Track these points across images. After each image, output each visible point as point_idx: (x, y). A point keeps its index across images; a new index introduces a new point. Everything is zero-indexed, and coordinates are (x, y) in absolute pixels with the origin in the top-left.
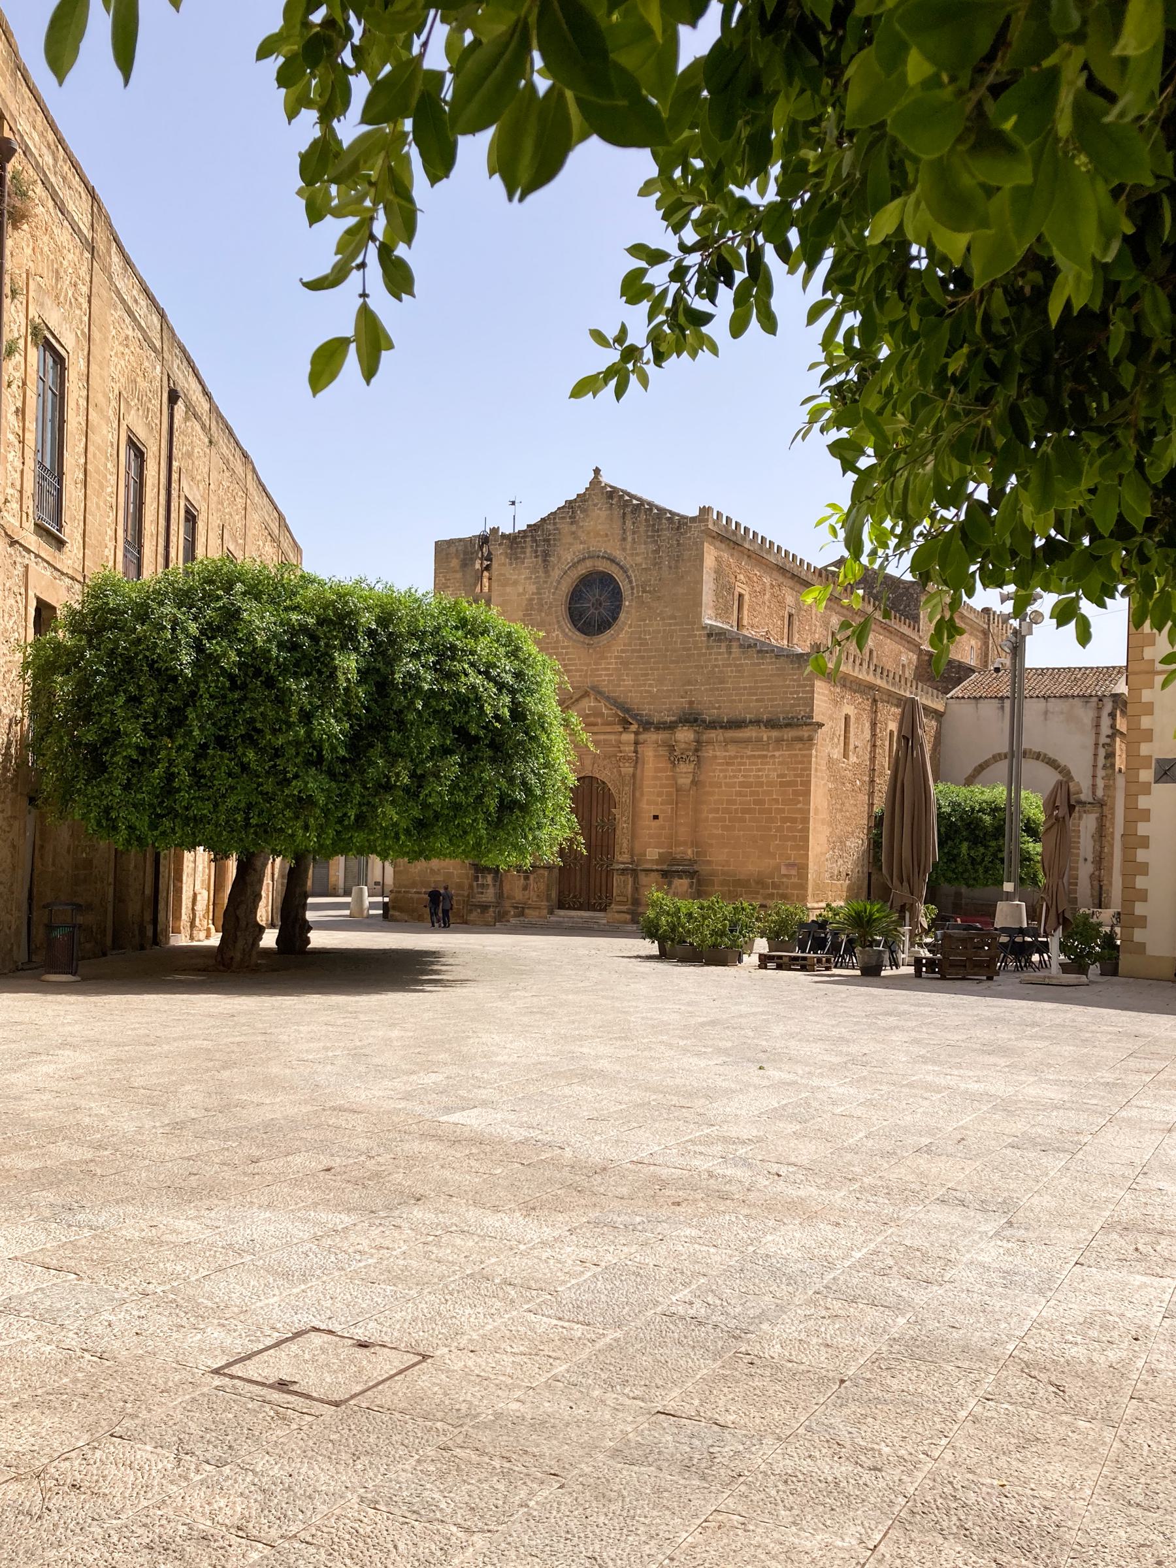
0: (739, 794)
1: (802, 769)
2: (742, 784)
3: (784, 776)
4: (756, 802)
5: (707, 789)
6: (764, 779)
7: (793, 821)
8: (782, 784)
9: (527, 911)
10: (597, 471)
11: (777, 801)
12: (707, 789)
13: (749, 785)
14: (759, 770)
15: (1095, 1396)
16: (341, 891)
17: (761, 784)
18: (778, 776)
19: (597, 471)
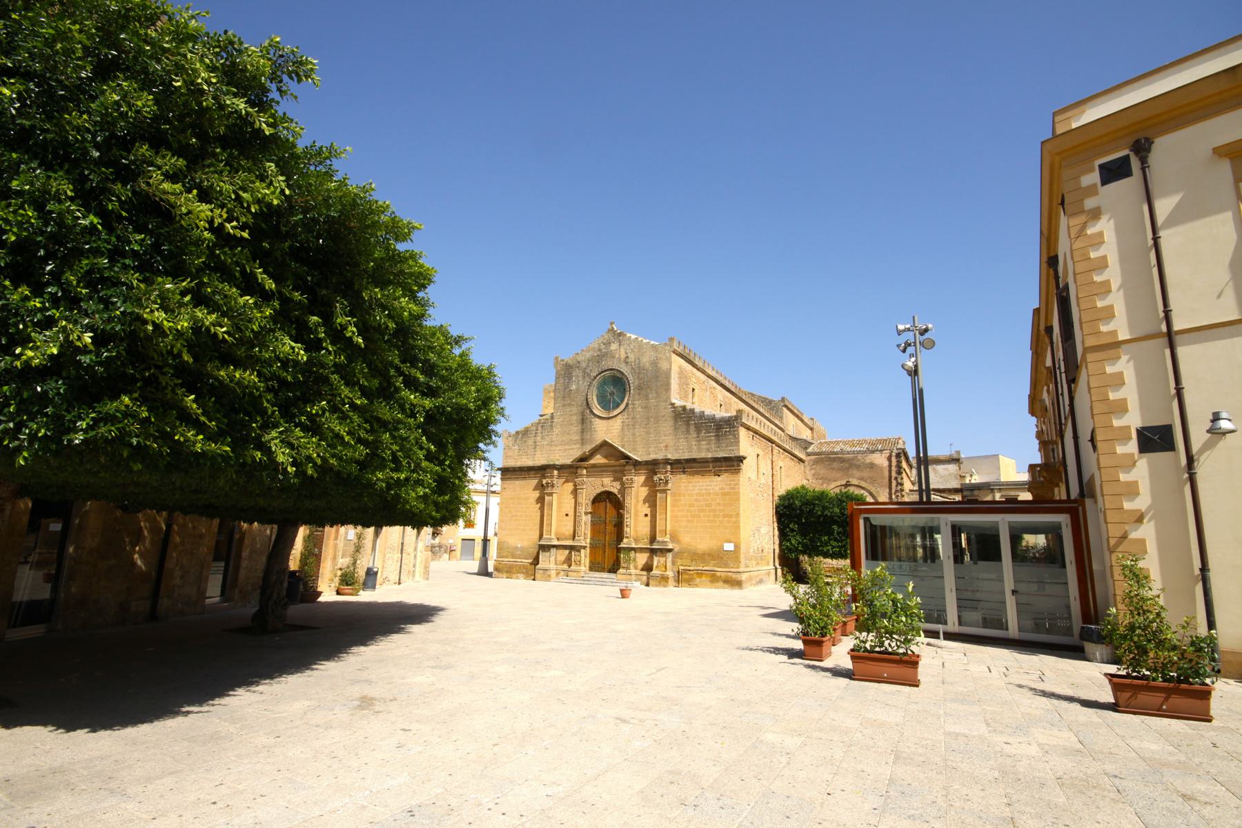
0: (696, 500)
2: (698, 494)
7: (731, 516)
17: (709, 494)
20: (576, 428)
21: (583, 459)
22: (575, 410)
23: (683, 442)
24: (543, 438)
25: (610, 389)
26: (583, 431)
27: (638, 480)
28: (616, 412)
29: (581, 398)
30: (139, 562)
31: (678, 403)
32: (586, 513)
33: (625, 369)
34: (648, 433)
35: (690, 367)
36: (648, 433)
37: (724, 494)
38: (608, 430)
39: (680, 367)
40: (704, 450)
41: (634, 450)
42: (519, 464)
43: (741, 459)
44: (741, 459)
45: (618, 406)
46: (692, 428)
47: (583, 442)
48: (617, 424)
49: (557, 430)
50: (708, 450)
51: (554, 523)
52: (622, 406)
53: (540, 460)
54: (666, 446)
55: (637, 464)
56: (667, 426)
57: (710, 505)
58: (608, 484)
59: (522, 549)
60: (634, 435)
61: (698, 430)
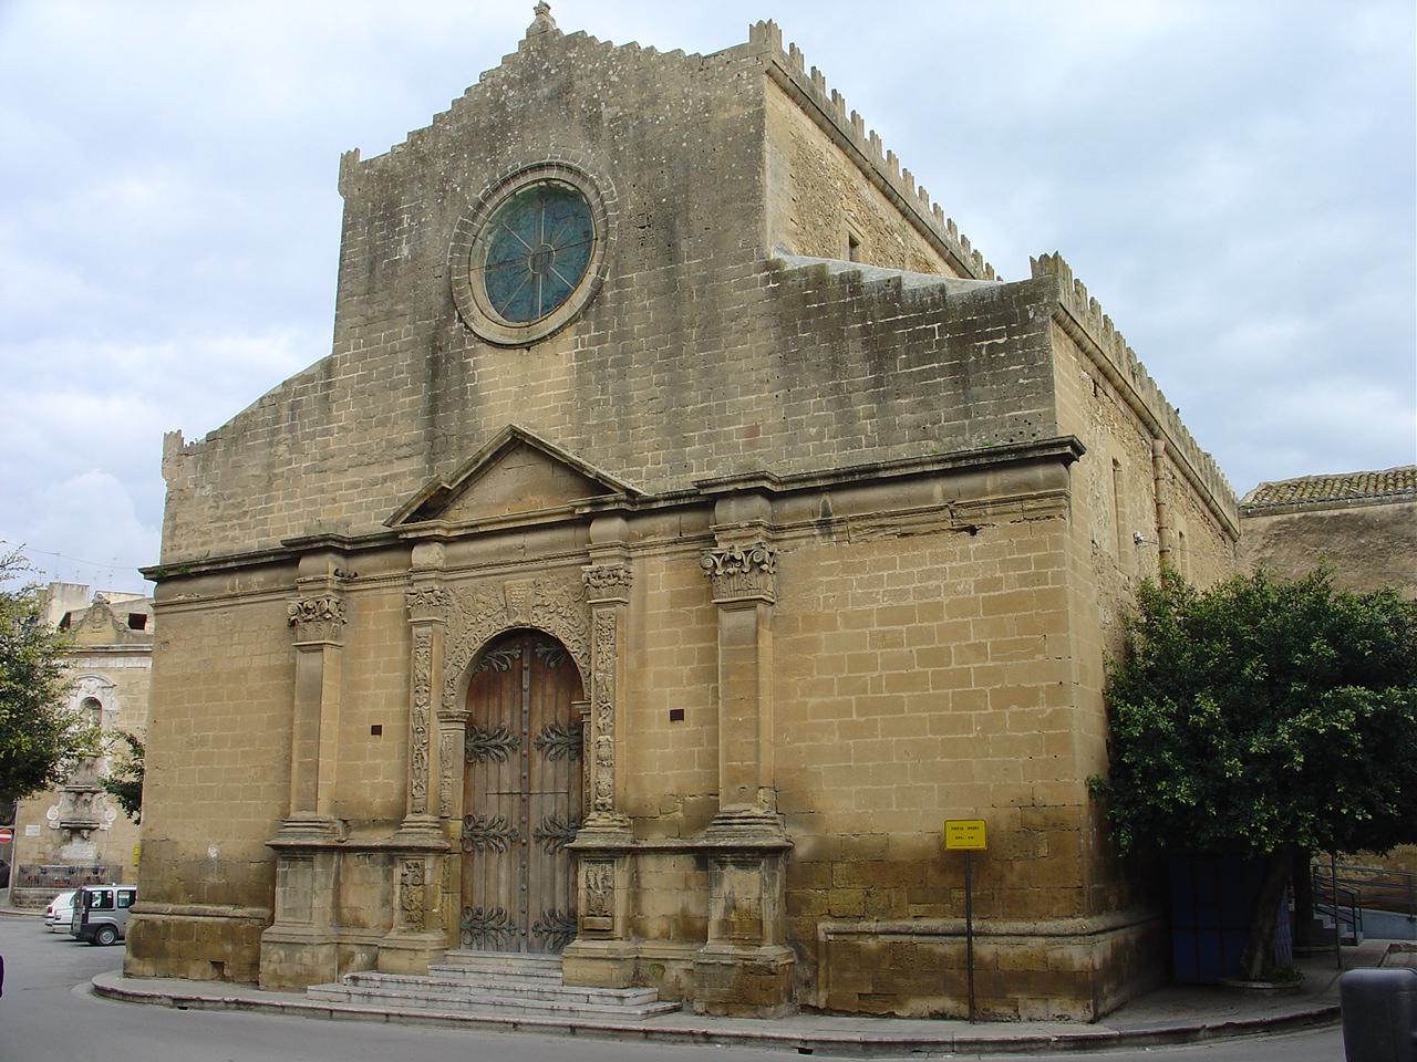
0: (882, 640)
1: (1040, 562)
2: (887, 616)
3: (994, 583)
4: (926, 658)
5: (686, 670)
6: (944, 599)
7: (1029, 697)
8: (994, 606)
9: (386, 959)
10: (542, 10)
11: (979, 649)
12: (686, 670)
13: (904, 616)
14: (929, 575)
15: (469, 167)
16: (714, 664)
17: (935, 611)
18: (980, 586)
19: (542, 10)
20: (408, 401)
21: (434, 503)
22: (405, 331)
23: (817, 409)
24: (295, 447)
25: (532, 239)
26: (434, 406)
27: (659, 575)
28: (554, 321)
29: (434, 286)
30: (1021, 734)
31: (794, 261)
32: (447, 718)
33: (585, 155)
34: (677, 387)
35: (834, 157)
36: (677, 387)
37: (997, 606)
38: (525, 387)
39: (799, 142)
40: (915, 425)
41: (625, 457)
42: (216, 549)
43: (1067, 452)
44: (1067, 452)
45: (563, 296)
46: (854, 351)
47: (434, 446)
48: (557, 365)
49: (344, 414)
50: (922, 432)
51: (328, 762)
52: (580, 297)
53: (283, 524)
54: (753, 432)
55: (637, 508)
56: (750, 354)
57: (940, 657)
58: (531, 594)
59: (222, 864)
60: (624, 399)
61: (880, 356)
